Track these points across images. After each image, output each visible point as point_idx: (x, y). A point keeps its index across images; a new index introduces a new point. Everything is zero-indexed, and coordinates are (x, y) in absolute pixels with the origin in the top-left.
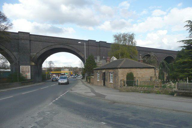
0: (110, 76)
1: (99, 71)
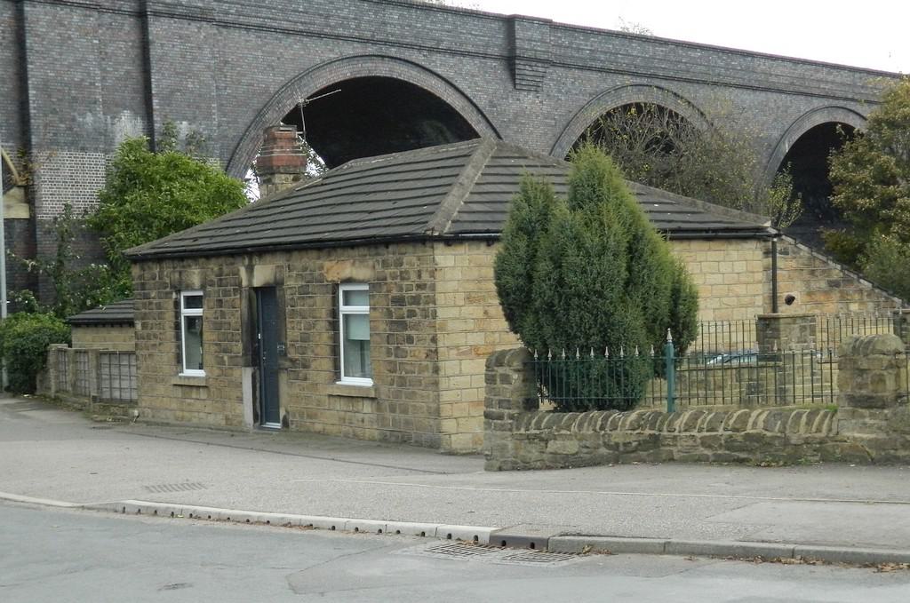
0: (334, 326)
1: (195, 275)
